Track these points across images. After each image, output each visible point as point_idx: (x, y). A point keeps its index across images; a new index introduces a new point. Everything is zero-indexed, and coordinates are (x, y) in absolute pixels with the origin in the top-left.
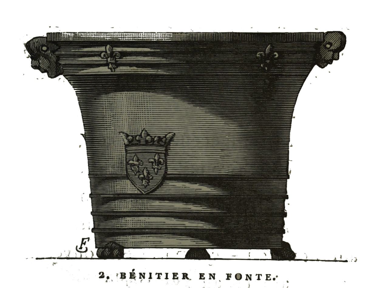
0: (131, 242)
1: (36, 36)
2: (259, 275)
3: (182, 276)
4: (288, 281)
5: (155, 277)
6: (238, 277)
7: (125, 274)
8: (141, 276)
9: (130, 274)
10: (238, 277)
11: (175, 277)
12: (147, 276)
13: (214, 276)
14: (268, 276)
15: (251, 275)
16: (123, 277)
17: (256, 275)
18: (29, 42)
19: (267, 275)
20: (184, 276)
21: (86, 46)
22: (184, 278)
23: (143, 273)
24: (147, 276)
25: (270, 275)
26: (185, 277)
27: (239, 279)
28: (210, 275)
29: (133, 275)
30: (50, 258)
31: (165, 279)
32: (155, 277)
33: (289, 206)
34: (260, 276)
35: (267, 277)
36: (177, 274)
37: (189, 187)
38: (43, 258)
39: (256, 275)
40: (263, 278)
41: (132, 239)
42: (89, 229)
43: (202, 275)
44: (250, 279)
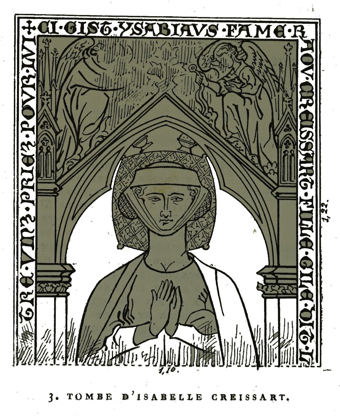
1: (84, 309)
2: (70, 395)
3: (220, 397)
4: (202, 397)
7: (166, 395)
9: (161, 396)
11: (199, 398)
14: (199, 396)
16: (164, 398)
19: (197, 395)
20: (272, 398)
22: (222, 399)
25: (201, 395)
26: (273, 398)
29: (234, 397)
30: (164, 340)
34: (71, 395)
35: (197, 397)
36: (235, 395)
37: (162, 351)
38: (278, 217)
39: (68, 394)
40: (95, 397)
43: (233, 396)
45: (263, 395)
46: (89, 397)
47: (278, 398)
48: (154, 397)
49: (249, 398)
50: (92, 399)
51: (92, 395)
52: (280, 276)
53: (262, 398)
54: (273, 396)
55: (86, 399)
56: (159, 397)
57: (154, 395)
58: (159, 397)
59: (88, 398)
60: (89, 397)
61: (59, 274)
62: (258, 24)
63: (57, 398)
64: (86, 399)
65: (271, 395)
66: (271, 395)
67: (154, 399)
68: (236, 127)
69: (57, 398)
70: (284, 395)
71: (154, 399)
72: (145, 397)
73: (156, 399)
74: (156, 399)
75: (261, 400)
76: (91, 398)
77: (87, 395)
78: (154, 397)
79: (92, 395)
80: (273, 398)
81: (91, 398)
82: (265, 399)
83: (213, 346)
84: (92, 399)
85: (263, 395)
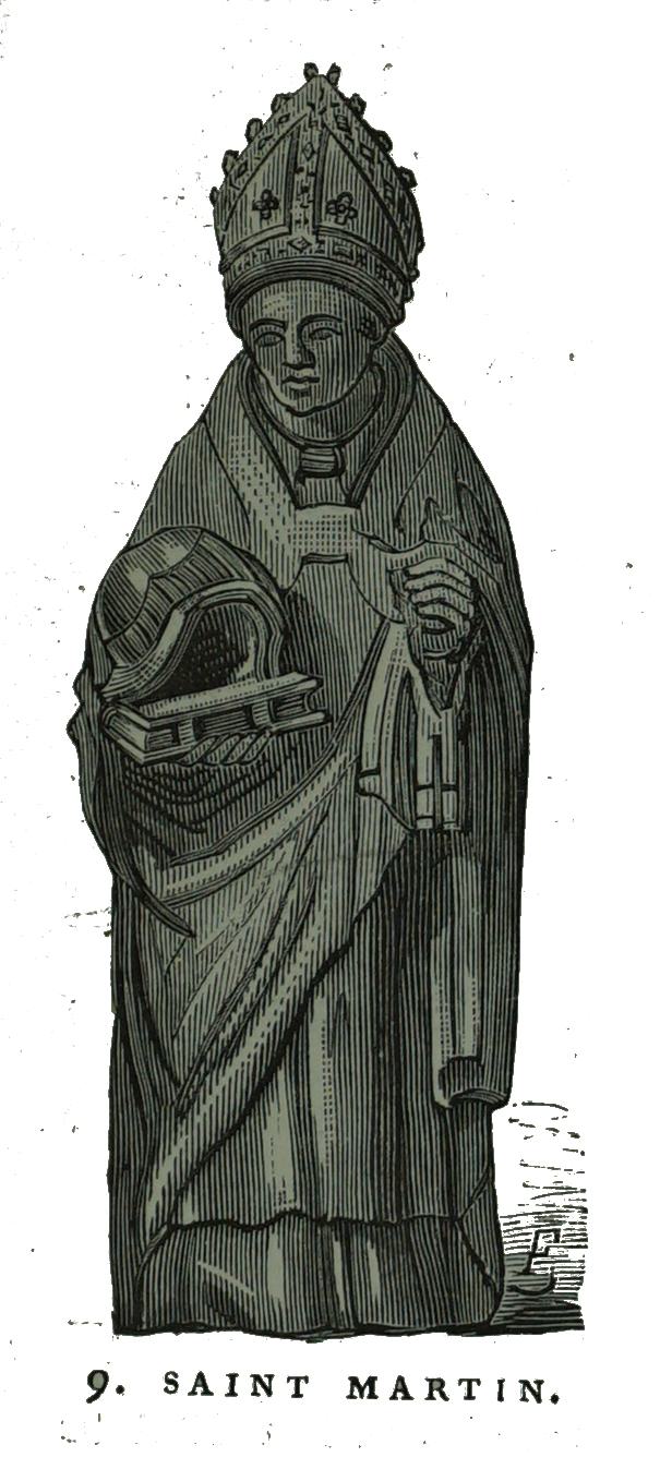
0: (318, 523)
2: (298, 1380)
5: (218, 1384)
6: (263, 1384)
8: (259, 1386)
10: (263, 1384)
12: (244, 1385)
13: (539, 1388)
15: (270, 1377)
17: (461, 1381)
18: (116, 1317)
21: (119, 1322)
23: (266, 1376)
24: (244, 1385)
27: (98, 1375)
28: (257, 1378)
31: (227, 1395)
32: (218, 1384)
33: (424, 261)
39: (289, 1379)
40: (385, 1387)
41: (287, 534)
42: (73, 778)
44: (269, 1392)
45: (201, 1376)
46: (361, 1390)
47: (455, 1391)
48: (401, 1389)
49: (176, 1385)
50: (372, 1396)
51: (371, 1381)
52: (201, 804)
53: (196, 1385)
54: (437, 1385)
55: (351, 1396)
56: (418, 1388)
57: (401, 1379)
58: (418, 1388)
59: (356, 1393)
60: (361, 1390)
61: (180, 808)
62: (294, 222)
63: (120, 1390)
64: (351, 1396)
65: (431, 1381)
66: (431, 1381)
67: (400, 1395)
68: (566, 1110)
69: (555, 1399)
70: (306, 1379)
71: (400, 1395)
72: (169, 1381)
73: (407, 1397)
74: (407, 1397)
75: (193, 1393)
76: (367, 1391)
77: (354, 1381)
78: (401, 1389)
79: (371, 1381)
80: (436, 1394)
81: (367, 1391)
82: (207, 1392)
83: (185, 1121)
84: (372, 1396)
85: (201, 1376)
